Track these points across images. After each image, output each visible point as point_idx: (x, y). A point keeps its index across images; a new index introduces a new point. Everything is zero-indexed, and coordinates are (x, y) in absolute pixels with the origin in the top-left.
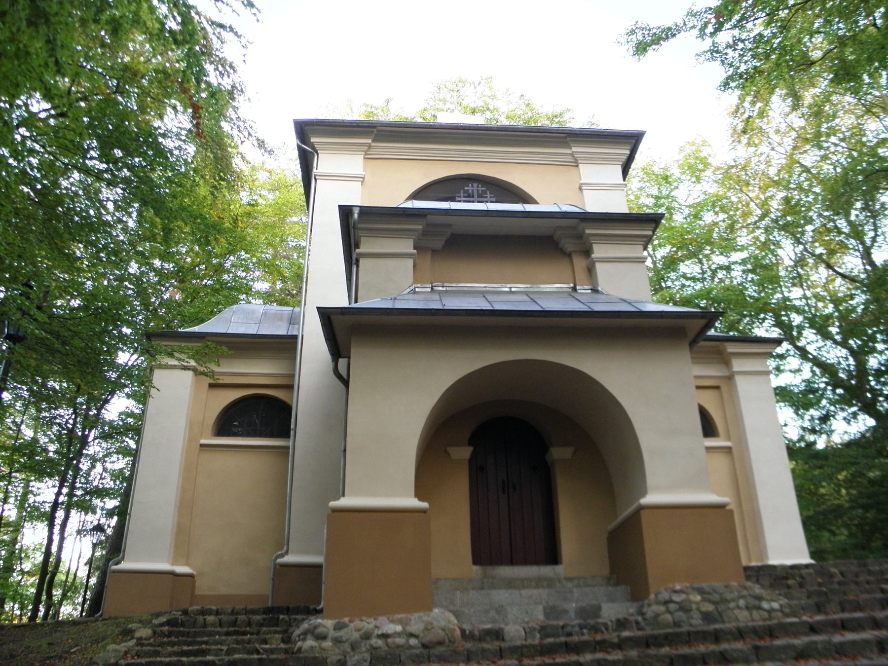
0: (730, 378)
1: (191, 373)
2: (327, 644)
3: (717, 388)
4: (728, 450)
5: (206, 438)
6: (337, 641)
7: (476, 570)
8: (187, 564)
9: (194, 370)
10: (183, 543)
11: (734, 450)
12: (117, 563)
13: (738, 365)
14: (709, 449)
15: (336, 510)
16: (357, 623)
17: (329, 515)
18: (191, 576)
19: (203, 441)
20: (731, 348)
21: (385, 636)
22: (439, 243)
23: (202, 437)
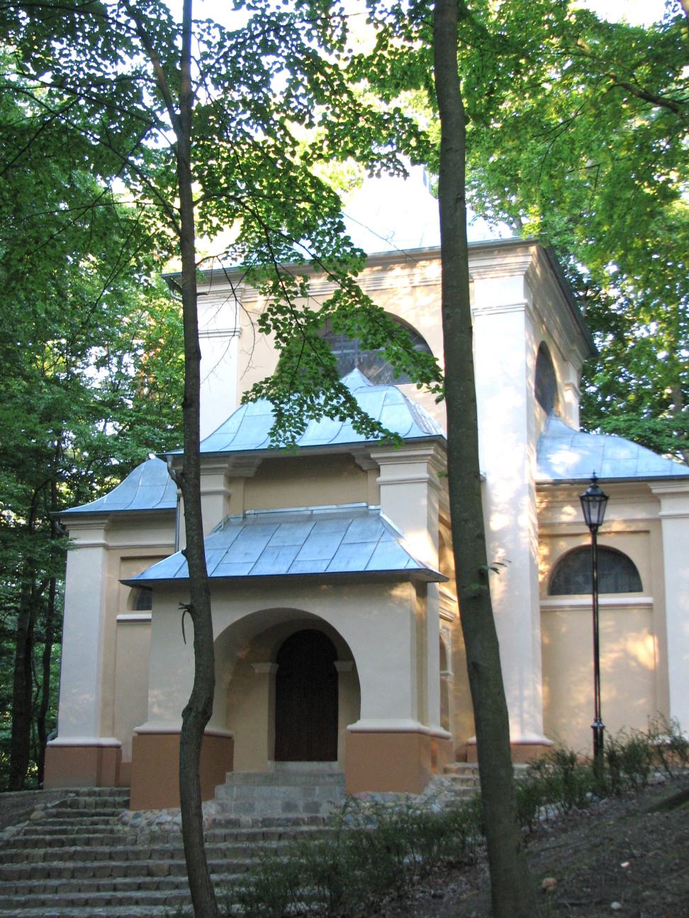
0: (658, 521)
1: (101, 550)
2: (127, 829)
3: (647, 532)
4: (650, 606)
5: (124, 613)
6: (133, 826)
7: (271, 765)
8: (113, 735)
9: (106, 547)
10: (109, 719)
11: (654, 607)
12: (53, 738)
13: (667, 508)
14: (129, 786)
15: (141, 734)
16: (149, 814)
17: (134, 739)
18: (118, 747)
19: (120, 617)
20: (657, 489)
21: (159, 824)
22: (251, 472)
23: (118, 611)
